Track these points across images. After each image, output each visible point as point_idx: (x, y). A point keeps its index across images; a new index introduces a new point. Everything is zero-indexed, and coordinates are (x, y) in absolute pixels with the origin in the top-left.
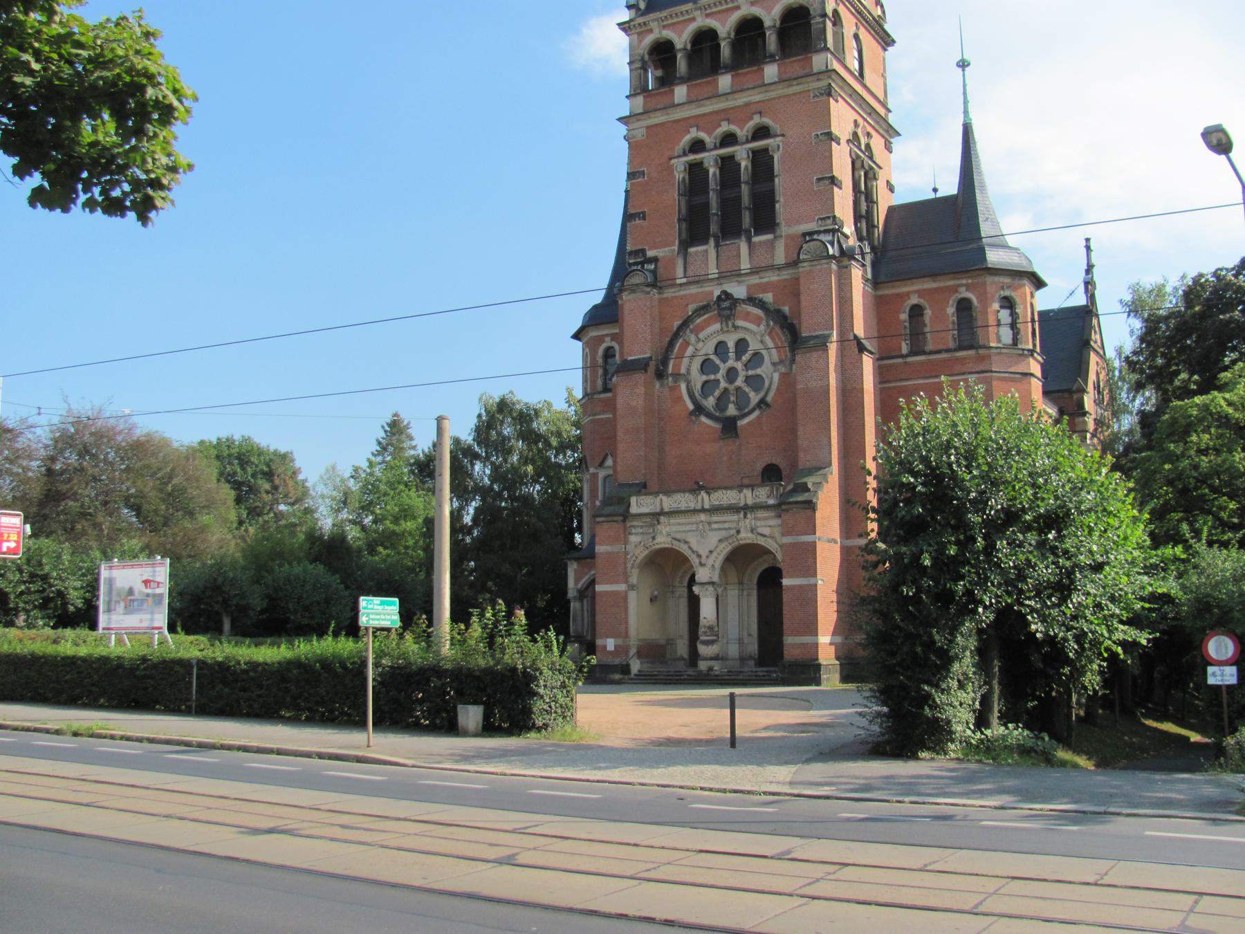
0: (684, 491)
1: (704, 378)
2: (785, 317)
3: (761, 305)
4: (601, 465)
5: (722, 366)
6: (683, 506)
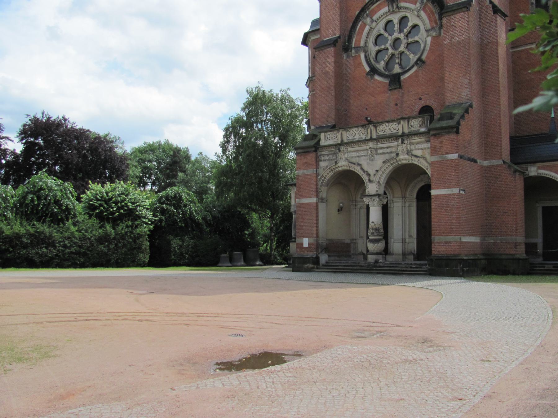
0: (357, 127)
1: (377, 48)
5: (390, 38)
6: (357, 138)
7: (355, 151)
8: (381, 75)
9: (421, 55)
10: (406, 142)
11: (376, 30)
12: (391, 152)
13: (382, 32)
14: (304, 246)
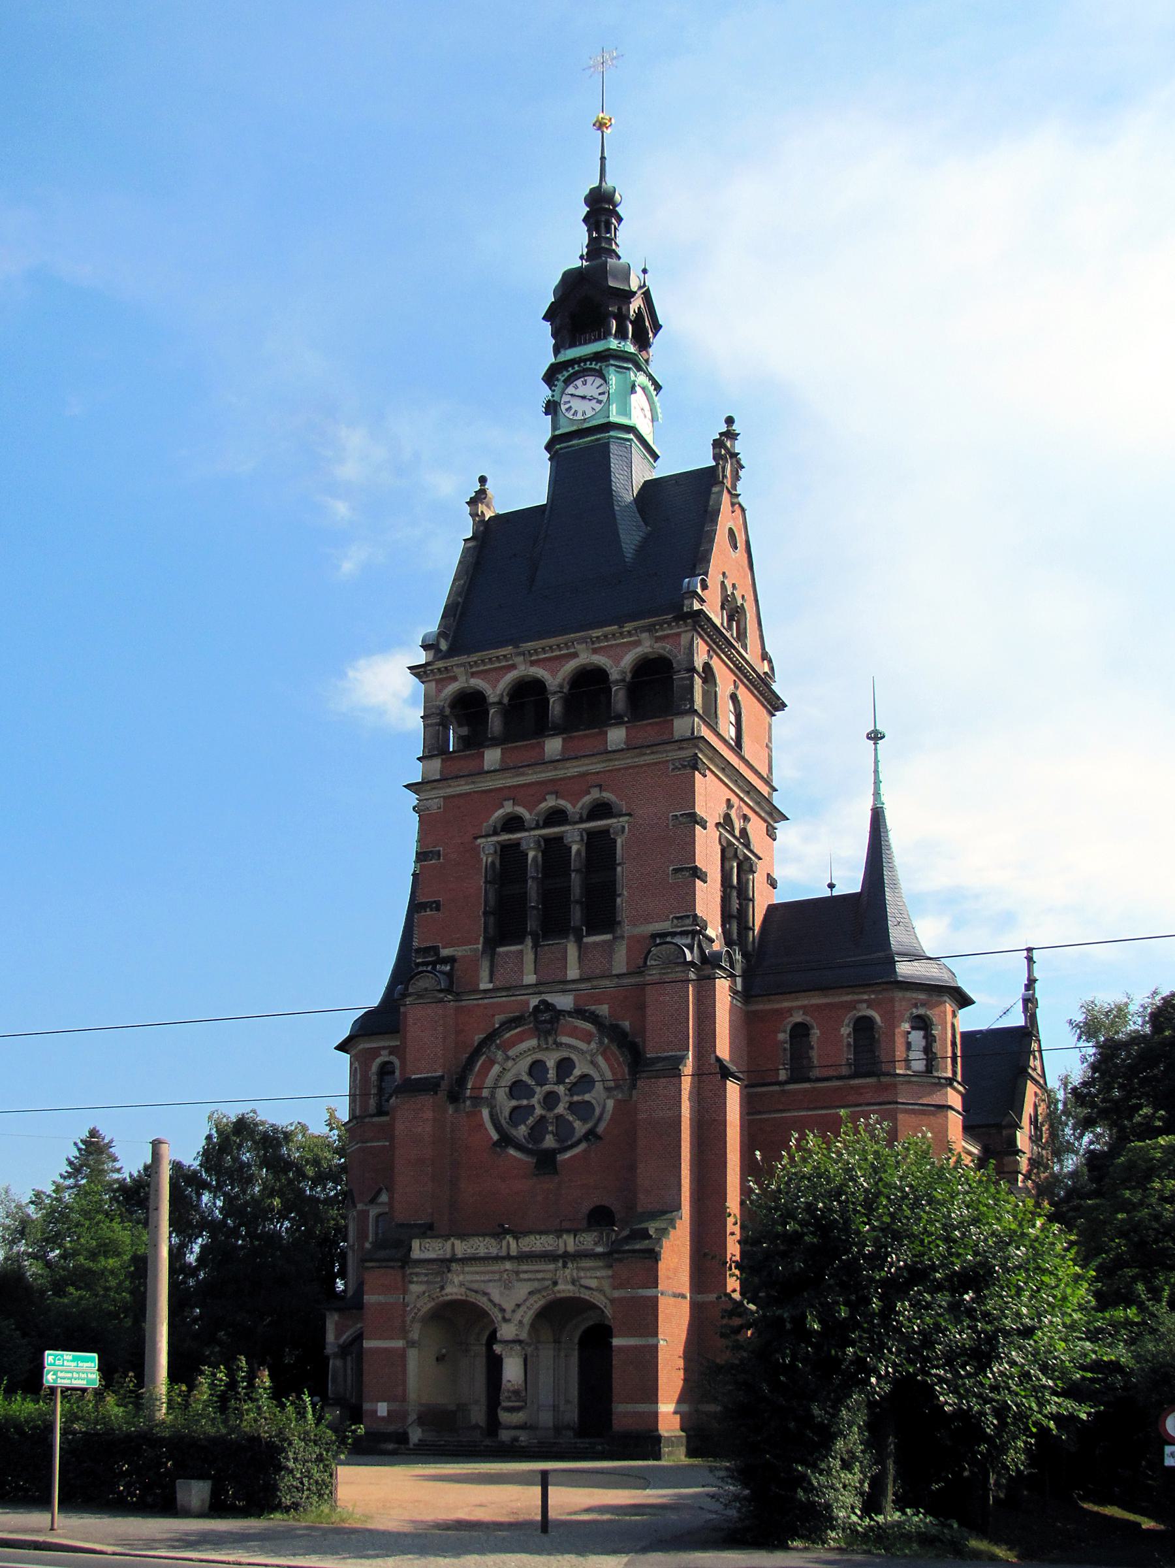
0: (484, 1235)
1: (514, 1103)
2: (624, 1034)
3: (594, 1018)
4: (373, 1201)
5: (538, 1089)
6: (482, 1252)
7: (477, 1273)
8: (519, 1147)
9: (596, 1125)
10: (570, 1265)
11: (513, 1071)
12: (543, 1279)
13: (525, 1078)
14: (50, 1356)
